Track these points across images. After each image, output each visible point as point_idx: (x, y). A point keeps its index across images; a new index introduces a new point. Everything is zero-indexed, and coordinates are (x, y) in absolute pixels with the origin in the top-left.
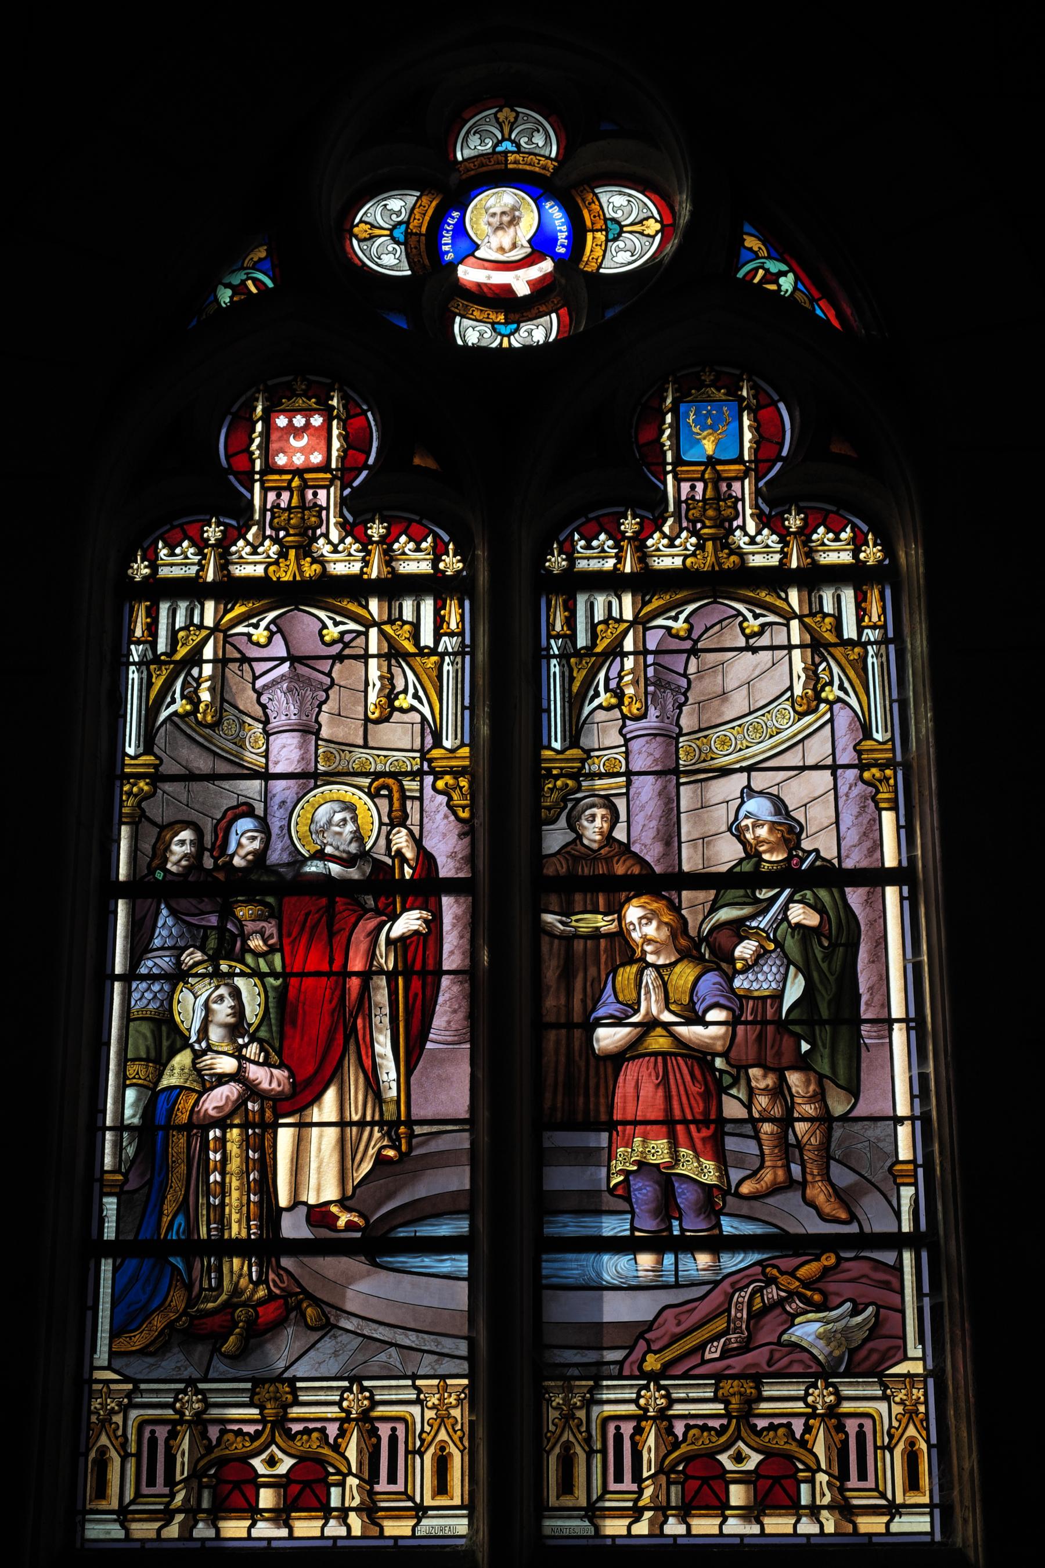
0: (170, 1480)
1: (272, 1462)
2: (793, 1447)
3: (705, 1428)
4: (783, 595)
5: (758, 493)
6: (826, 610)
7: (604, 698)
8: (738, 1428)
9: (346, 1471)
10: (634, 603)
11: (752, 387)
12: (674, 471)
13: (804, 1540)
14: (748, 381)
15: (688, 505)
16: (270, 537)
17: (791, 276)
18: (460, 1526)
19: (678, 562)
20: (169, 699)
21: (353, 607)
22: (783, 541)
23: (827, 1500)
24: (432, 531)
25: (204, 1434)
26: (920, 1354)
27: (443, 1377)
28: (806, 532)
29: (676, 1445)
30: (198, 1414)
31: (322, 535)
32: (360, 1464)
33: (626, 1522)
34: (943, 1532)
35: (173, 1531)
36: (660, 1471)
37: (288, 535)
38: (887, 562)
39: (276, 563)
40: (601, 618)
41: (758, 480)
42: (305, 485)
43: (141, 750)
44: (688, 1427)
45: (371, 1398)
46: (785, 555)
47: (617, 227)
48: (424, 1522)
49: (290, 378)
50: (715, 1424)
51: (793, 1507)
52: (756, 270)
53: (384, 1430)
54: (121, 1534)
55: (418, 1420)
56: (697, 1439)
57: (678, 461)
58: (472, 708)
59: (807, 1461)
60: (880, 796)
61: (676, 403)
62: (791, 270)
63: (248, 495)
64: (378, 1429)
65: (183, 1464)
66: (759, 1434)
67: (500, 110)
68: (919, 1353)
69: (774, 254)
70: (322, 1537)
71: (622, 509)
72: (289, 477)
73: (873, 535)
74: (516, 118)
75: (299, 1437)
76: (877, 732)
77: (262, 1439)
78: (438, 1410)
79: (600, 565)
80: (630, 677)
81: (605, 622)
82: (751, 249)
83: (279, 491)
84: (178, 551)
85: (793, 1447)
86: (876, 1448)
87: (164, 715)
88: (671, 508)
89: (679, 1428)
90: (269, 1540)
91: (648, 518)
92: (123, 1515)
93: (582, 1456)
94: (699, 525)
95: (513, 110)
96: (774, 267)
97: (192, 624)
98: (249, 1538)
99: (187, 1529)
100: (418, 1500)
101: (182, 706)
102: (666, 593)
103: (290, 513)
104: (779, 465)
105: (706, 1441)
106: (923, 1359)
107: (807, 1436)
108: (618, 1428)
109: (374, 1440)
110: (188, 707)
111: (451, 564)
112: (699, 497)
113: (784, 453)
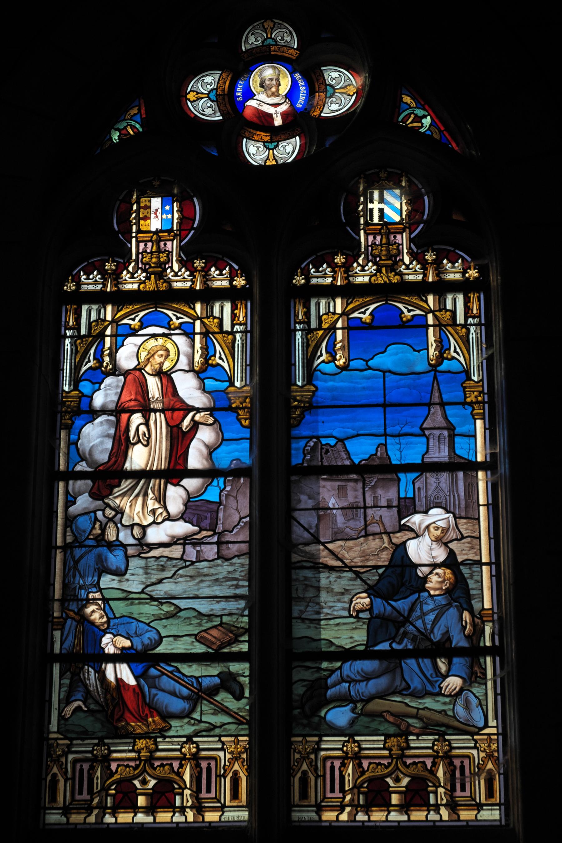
0: (342, 789)
1: (397, 780)
2: (426, 774)
3: (128, 766)
4: (192, 306)
5: (411, 240)
6: (448, 308)
7: (324, 357)
8: (144, 765)
9: (184, 787)
10: (342, 303)
11: (407, 181)
12: (136, 237)
13: (432, 824)
14: (364, 179)
15: (372, 248)
16: (141, 268)
17: (429, 118)
18: (244, 815)
19: (135, 286)
20: (319, 354)
21: (186, 309)
22: (424, 268)
23: (189, 804)
24: (461, 256)
25: (360, 765)
26: (495, 724)
27: (236, 736)
28: (206, 270)
29: (363, 773)
30: (446, 753)
31: (169, 267)
32: (191, 782)
33: (336, 813)
34: (506, 820)
35: (344, 817)
36: (355, 786)
37: (381, 259)
38: (248, 286)
39: (144, 282)
40: (95, 319)
41: (410, 233)
42: (159, 240)
43: (72, 387)
44: (118, 766)
45: (197, 747)
46: (425, 275)
47: (211, 96)
48: (482, 812)
49: (151, 178)
50: (385, 762)
51: (171, 806)
52: (409, 114)
53: (204, 764)
54: (317, 818)
55: (223, 758)
56: (375, 769)
57: (139, 231)
58: (251, 365)
59: (435, 782)
60: (475, 412)
61: (365, 190)
62: (429, 114)
63: (357, 238)
64: (362, 763)
65: (97, 783)
66: (408, 767)
67: (265, 21)
68: (495, 724)
69: (419, 105)
70: (172, 822)
71: (107, 258)
72: (152, 235)
73: (241, 271)
74: (274, 26)
75: (158, 768)
76: (237, 381)
77: (390, 769)
78: (234, 754)
79: (94, 288)
80: (340, 344)
81: (327, 314)
82: (406, 103)
83: (146, 242)
84: (91, 277)
85: (173, 776)
86: (216, 776)
87: (84, 369)
88: (134, 257)
89: (365, 763)
90: (399, 822)
91: (121, 262)
92: (66, 811)
93: (312, 778)
94: (378, 259)
95: (272, 21)
96: (419, 112)
97: (329, 311)
98: (387, 821)
99: (352, 816)
100: (478, 801)
101: (327, 358)
102: (130, 305)
103: (382, 247)
104: (193, 232)
105: (380, 771)
106: (497, 727)
107: (433, 768)
108: (332, 763)
109: (452, 768)
110: (330, 358)
111: (240, 282)
112: (378, 243)
113: (195, 226)
